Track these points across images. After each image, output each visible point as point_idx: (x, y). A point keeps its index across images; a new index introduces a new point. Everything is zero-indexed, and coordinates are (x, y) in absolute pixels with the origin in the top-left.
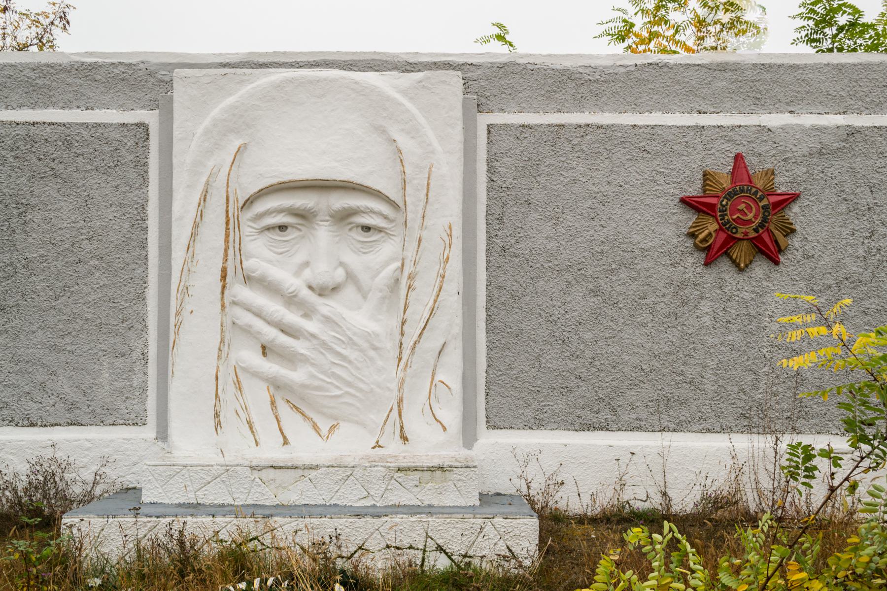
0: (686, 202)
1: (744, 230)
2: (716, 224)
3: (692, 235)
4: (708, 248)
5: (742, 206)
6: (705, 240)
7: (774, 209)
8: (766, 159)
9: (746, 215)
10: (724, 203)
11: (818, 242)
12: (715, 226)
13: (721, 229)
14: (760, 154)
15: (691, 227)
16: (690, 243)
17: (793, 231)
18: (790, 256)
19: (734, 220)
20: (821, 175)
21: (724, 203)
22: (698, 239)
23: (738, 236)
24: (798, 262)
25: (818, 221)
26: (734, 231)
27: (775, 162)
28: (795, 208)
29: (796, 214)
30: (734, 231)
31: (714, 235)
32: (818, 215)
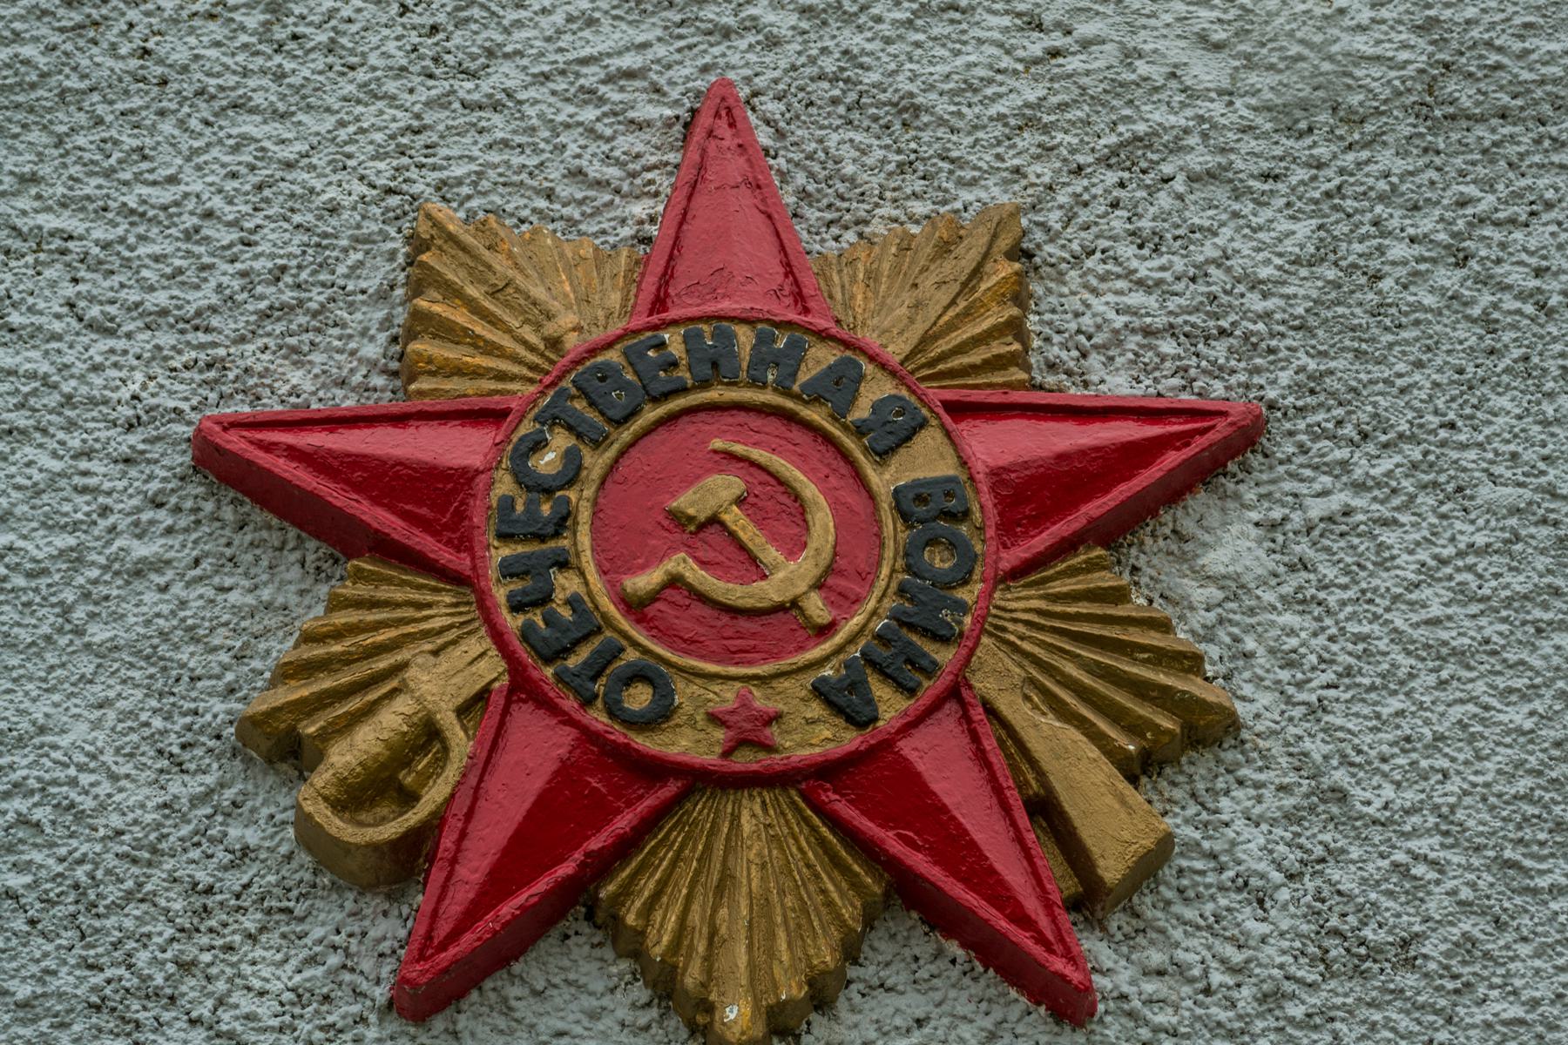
0: (256, 475)
1: (726, 697)
2: (478, 644)
3: (280, 746)
4: (406, 863)
5: (716, 492)
6: (379, 786)
7: (1010, 527)
8: (961, 145)
9: (755, 568)
10: (547, 461)
11: (1448, 827)
12: (474, 665)
13: (522, 687)
14: (909, 110)
15: (288, 672)
16: (264, 819)
17: (1209, 730)
18: (1192, 950)
19: (636, 607)
20: (1448, 278)
21: (547, 461)
22: (321, 778)
23: (684, 743)
24: (1271, 998)
25: (1442, 654)
26: (639, 698)
27: (1043, 171)
28: (1232, 538)
29: (1234, 587)
30: (639, 698)
31: (461, 743)
32: (1435, 600)
